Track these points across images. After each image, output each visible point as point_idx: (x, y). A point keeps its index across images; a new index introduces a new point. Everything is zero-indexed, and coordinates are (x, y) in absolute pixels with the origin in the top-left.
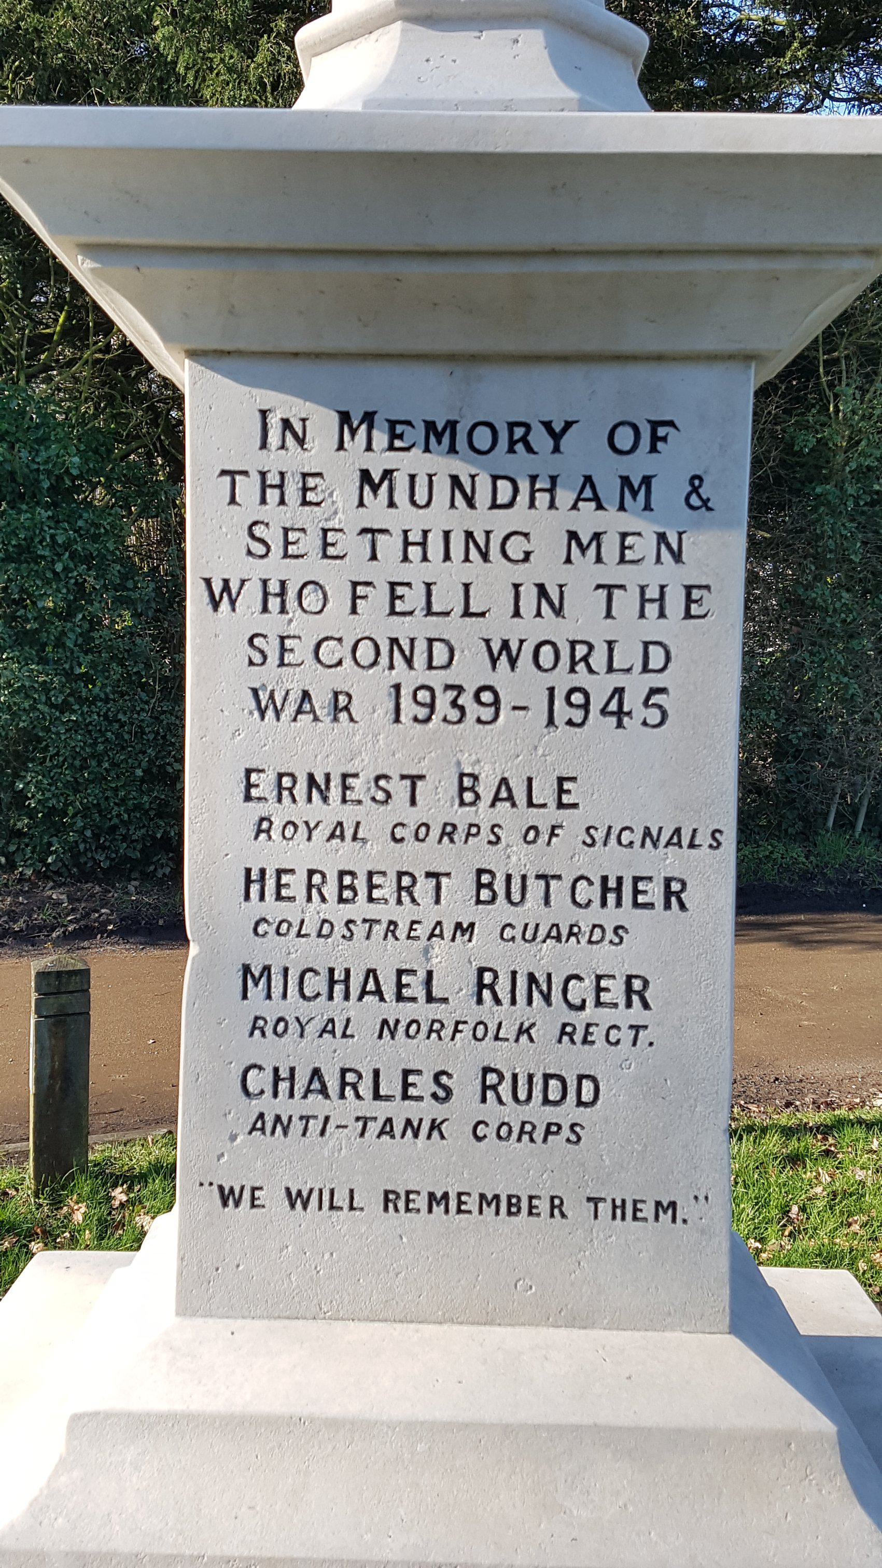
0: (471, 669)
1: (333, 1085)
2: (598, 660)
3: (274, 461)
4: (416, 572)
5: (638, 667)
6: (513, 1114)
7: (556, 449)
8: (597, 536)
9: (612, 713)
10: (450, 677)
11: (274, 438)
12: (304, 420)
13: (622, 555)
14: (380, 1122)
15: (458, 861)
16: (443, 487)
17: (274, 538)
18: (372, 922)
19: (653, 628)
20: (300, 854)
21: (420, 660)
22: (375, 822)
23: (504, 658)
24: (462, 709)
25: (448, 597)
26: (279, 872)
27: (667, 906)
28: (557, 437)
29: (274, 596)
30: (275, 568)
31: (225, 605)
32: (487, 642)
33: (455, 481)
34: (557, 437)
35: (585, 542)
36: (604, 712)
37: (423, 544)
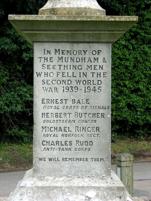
0: (74, 84)
1: (55, 143)
2: (92, 83)
3: (46, 56)
4: (66, 71)
5: (97, 84)
6: (80, 147)
7: (85, 54)
8: (91, 66)
9: (94, 90)
10: (71, 85)
11: (46, 53)
12: (86, 73)
13: (94, 68)
14: (62, 148)
15: (72, 111)
16: (69, 59)
17: (46, 66)
18: (60, 120)
19: (99, 79)
20: (50, 111)
21: (67, 83)
22: (60, 106)
23: (78, 83)
24: (73, 90)
25: (70, 74)
26: (47, 113)
27: (102, 117)
28: (85, 52)
29: (46, 74)
30: (46, 70)
31: (39, 76)
32: (76, 80)
33: (71, 58)
34: (85, 52)
35: (89, 66)
36: (93, 90)
37: (67, 67)
